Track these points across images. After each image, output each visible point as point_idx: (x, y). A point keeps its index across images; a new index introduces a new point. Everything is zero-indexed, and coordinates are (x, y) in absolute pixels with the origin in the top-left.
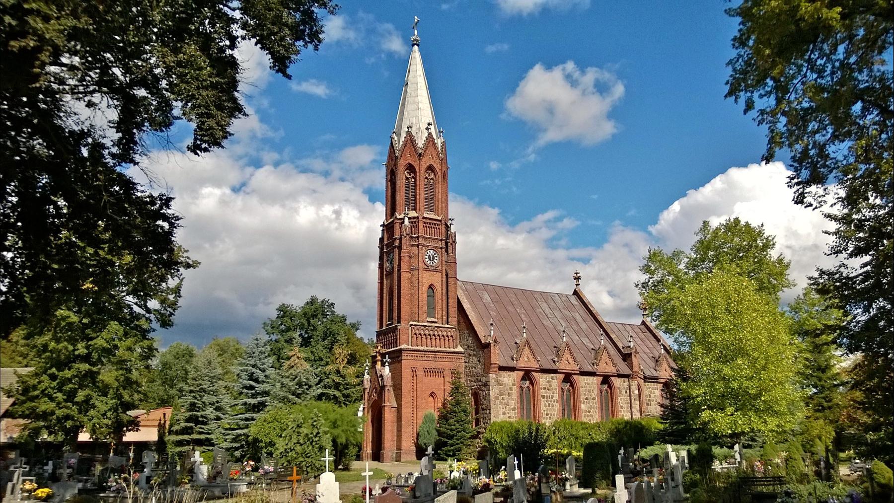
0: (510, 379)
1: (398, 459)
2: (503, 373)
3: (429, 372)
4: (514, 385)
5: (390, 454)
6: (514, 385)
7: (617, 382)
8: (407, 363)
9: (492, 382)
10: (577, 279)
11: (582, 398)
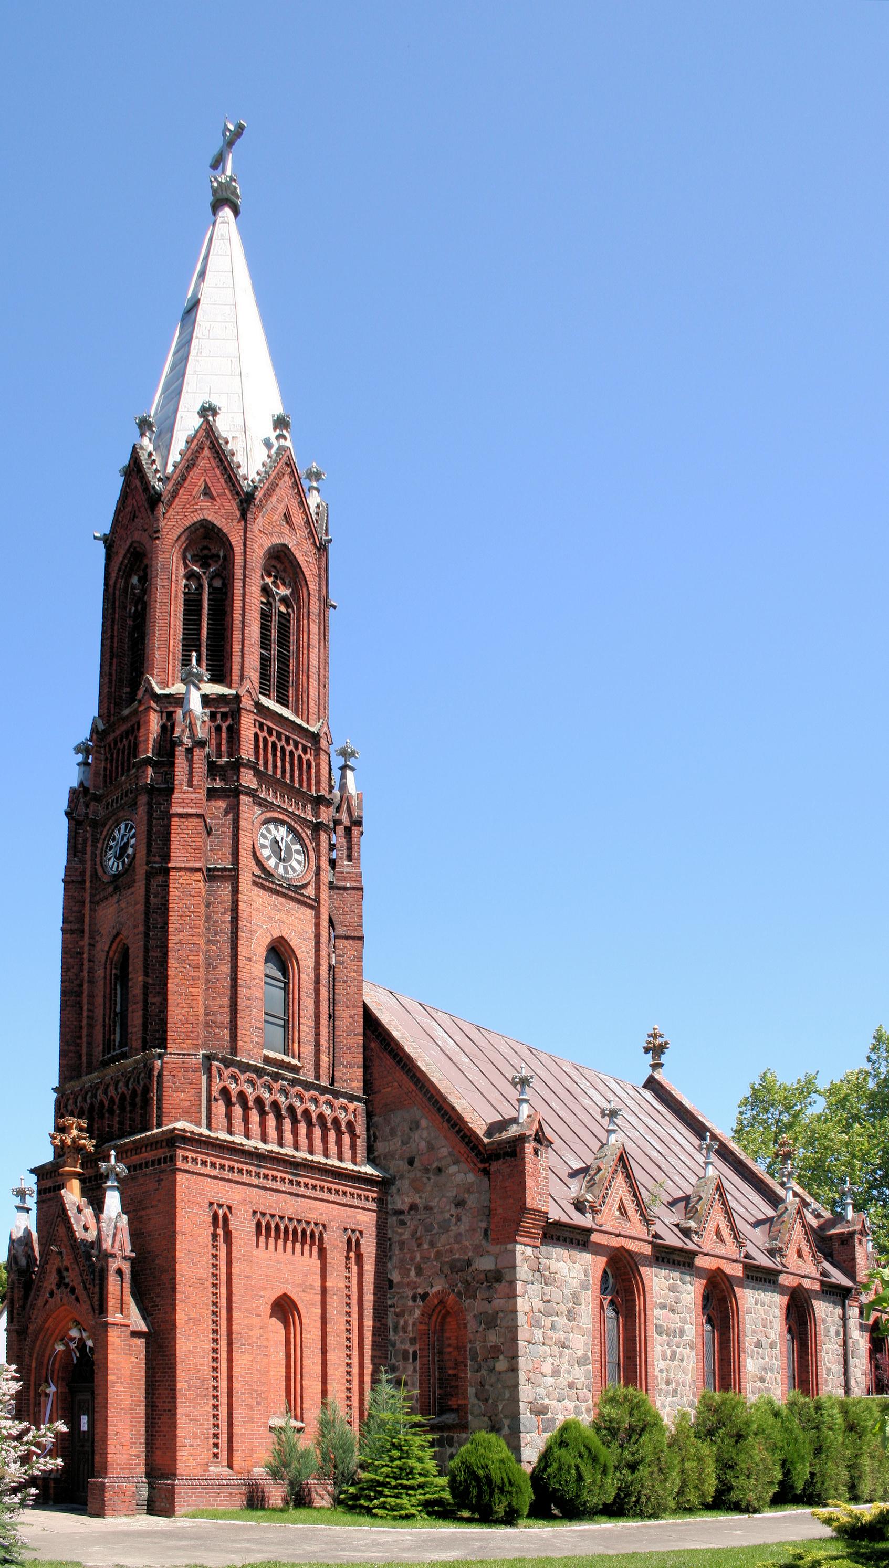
0: (576, 1270)
1: (159, 1503)
2: (558, 1252)
3: (269, 1229)
4: (585, 1287)
5: (129, 1488)
6: (585, 1287)
7: (823, 1309)
8: (196, 1192)
9: (523, 1271)
10: (656, 1049)
11: (748, 1341)
